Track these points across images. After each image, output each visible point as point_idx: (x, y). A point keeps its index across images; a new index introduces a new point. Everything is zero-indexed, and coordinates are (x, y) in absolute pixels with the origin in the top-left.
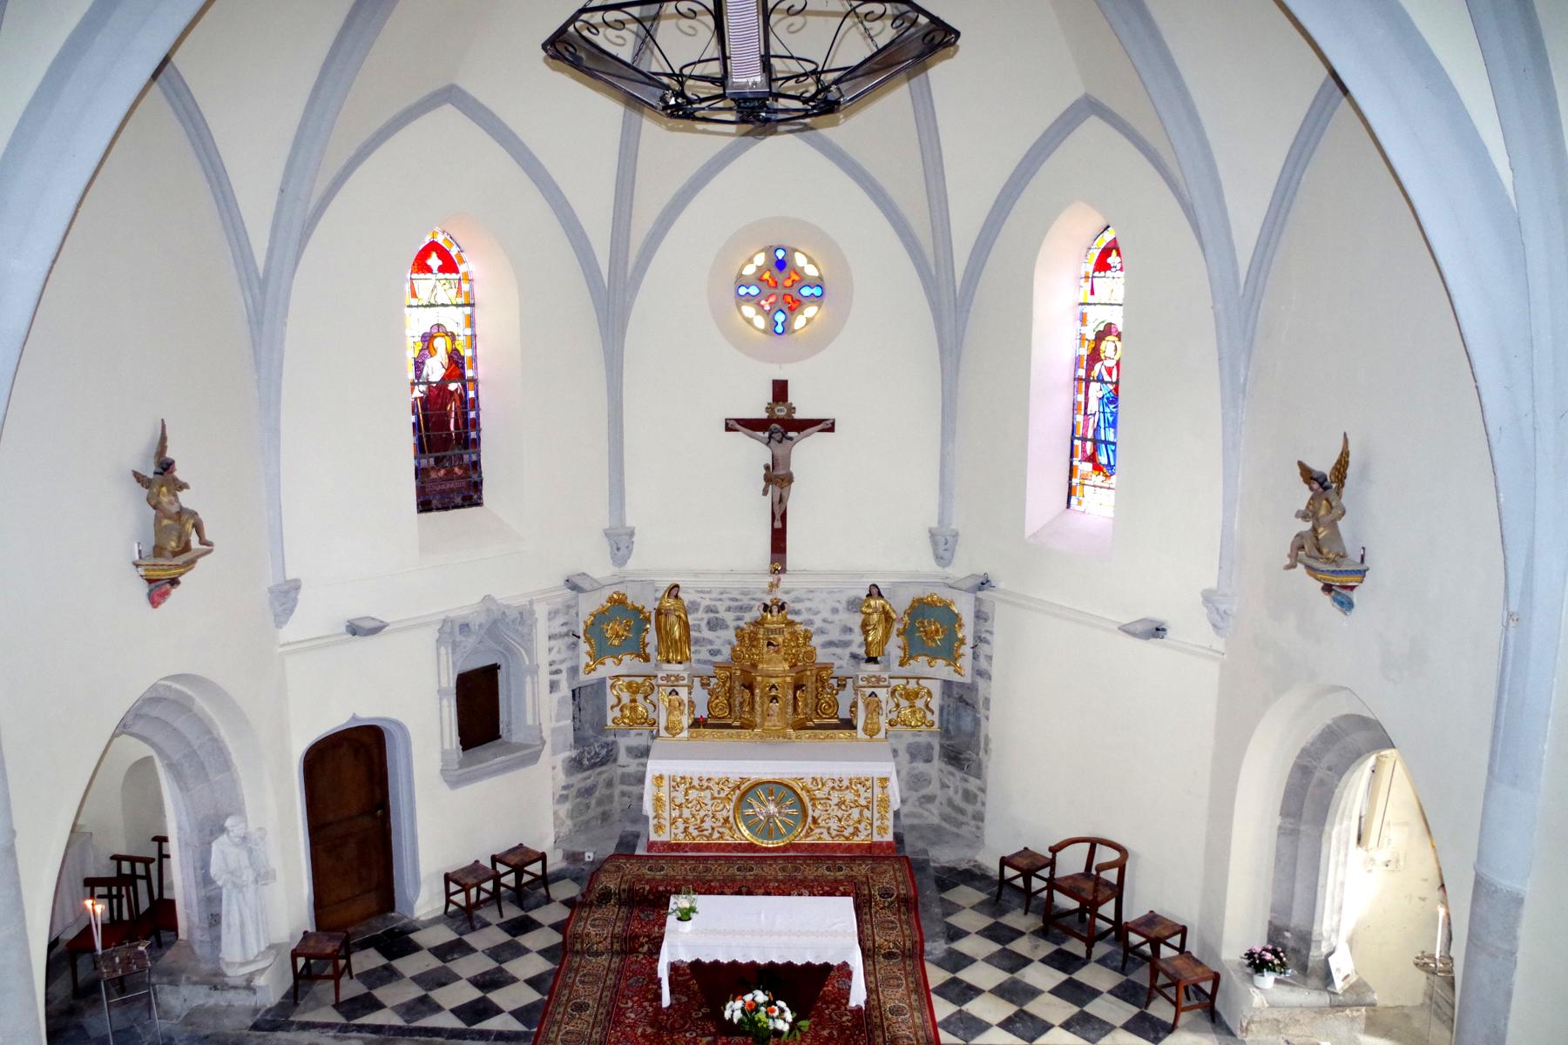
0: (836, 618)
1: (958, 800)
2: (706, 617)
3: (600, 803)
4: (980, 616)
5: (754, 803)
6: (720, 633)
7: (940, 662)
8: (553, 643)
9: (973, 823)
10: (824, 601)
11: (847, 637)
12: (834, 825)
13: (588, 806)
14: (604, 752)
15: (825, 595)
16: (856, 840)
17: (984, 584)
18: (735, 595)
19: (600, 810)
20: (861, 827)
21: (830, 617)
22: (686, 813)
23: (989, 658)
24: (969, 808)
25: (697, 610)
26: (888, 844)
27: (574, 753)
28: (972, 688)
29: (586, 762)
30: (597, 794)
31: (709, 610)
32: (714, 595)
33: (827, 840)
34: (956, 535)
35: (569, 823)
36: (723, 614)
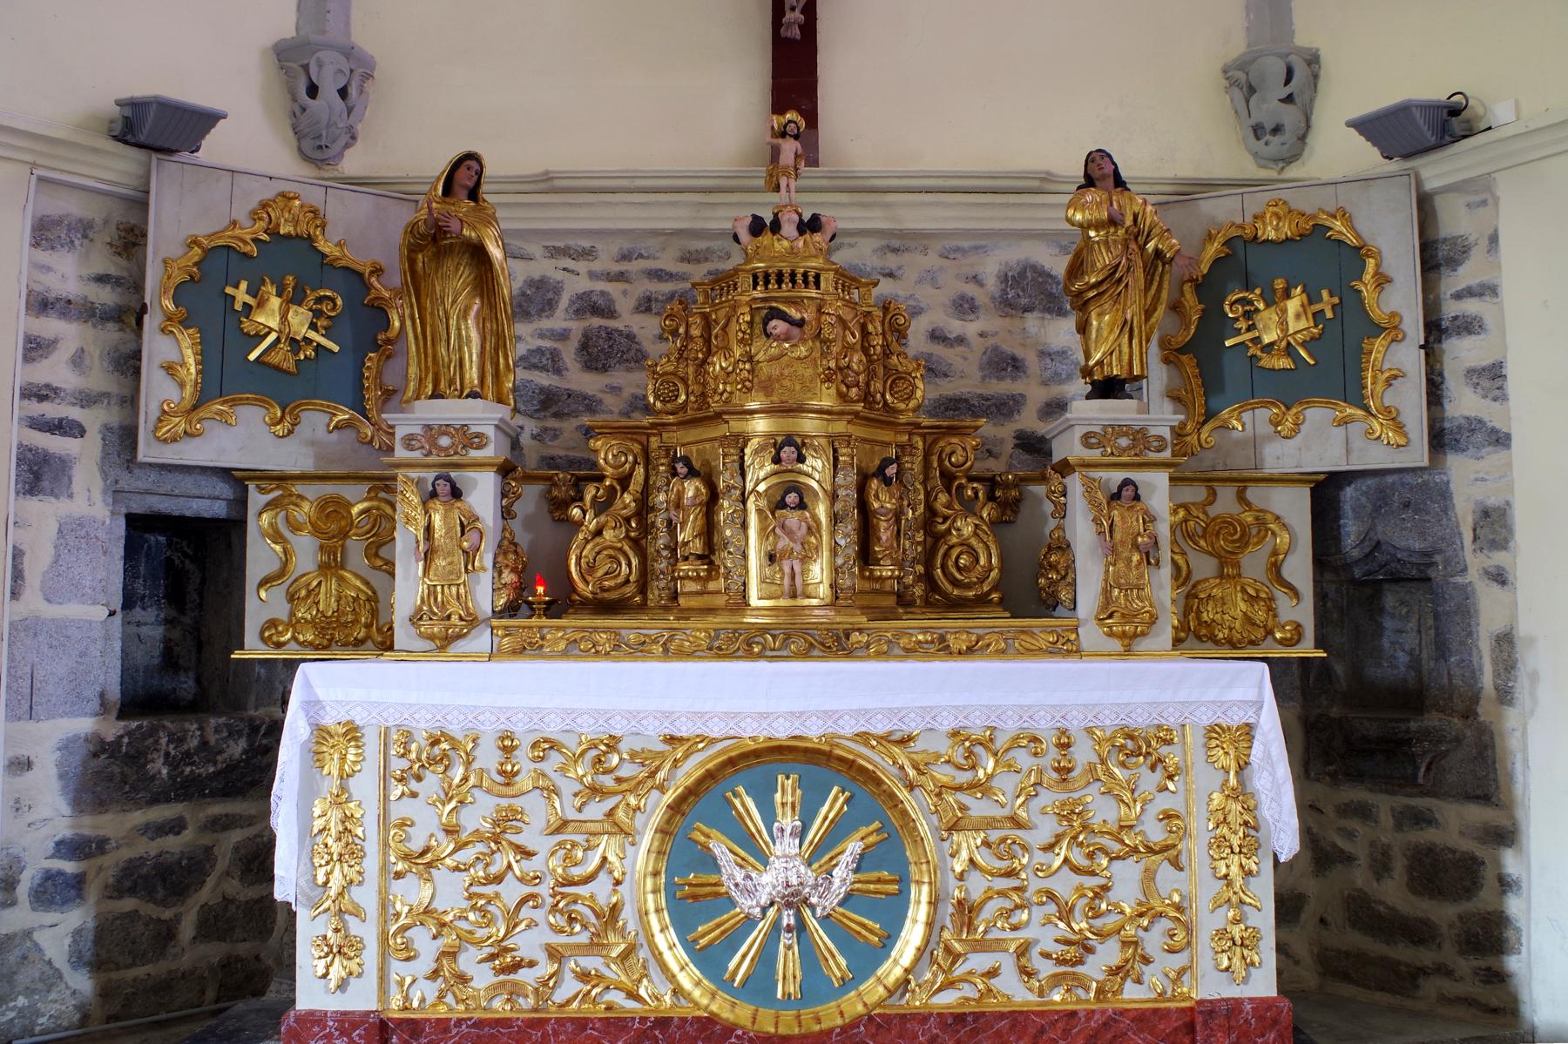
0: (971, 328)
1: (1394, 893)
2: (577, 327)
3: (213, 925)
4: (1434, 258)
5: (720, 848)
6: (618, 377)
7: (1316, 415)
8: (50, 326)
9: (1465, 965)
10: (931, 278)
11: (1002, 387)
12: (1045, 934)
13: (166, 935)
14: (237, 748)
15: (932, 260)
16: (1133, 994)
17: (1449, 122)
18: (668, 263)
19: (214, 952)
20: (1153, 941)
21: (955, 327)
22: (449, 893)
23: (1492, 376)
24: (1444, 913)
25: (549, 306)
26: (1262, 1004)
27: (113, 729)
28: (1417, 493)
29: (159, 767)
30: (206, 894)
31: (590, 306)
32: (604, 263)
33: (1015, 992)
34: (1313, 60)
35: (82, 983)
36: (628, 320)
